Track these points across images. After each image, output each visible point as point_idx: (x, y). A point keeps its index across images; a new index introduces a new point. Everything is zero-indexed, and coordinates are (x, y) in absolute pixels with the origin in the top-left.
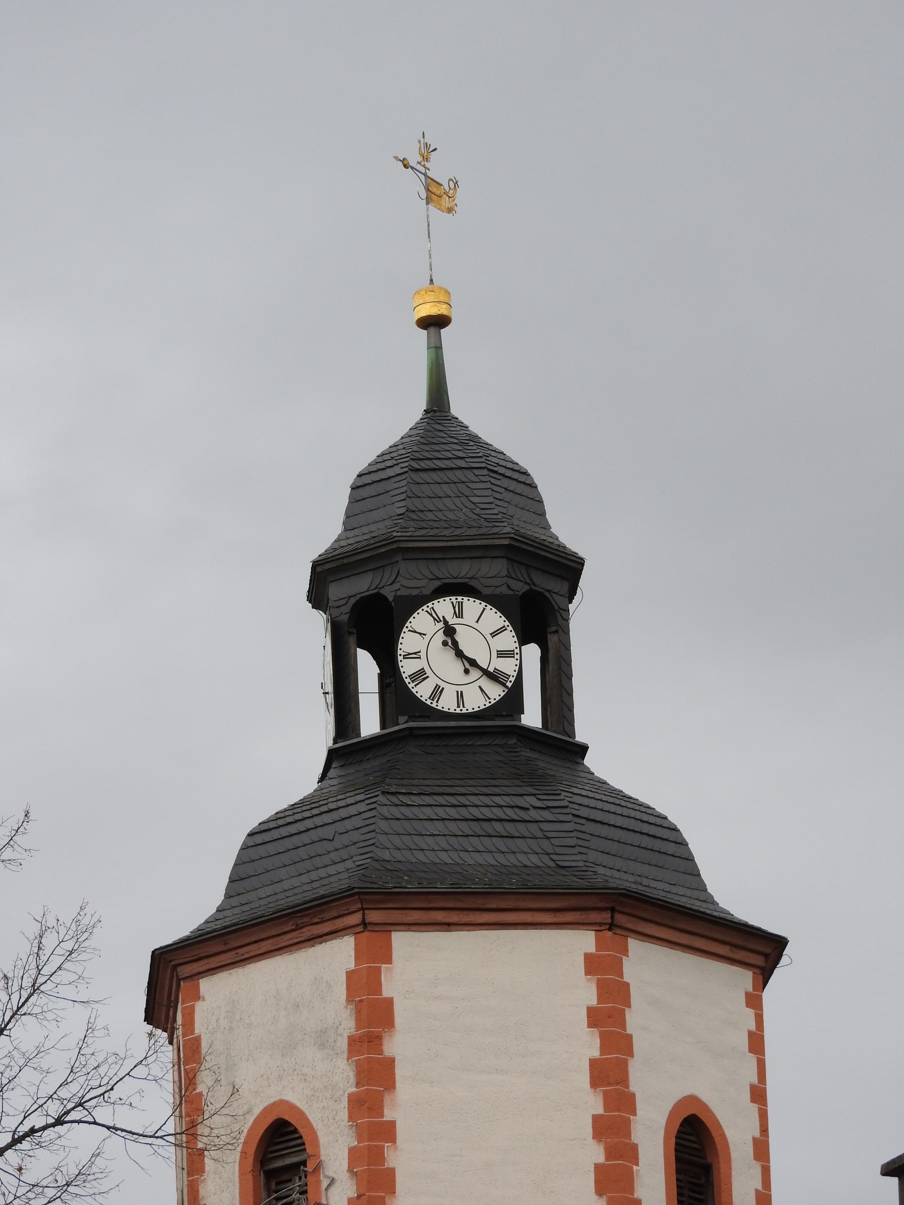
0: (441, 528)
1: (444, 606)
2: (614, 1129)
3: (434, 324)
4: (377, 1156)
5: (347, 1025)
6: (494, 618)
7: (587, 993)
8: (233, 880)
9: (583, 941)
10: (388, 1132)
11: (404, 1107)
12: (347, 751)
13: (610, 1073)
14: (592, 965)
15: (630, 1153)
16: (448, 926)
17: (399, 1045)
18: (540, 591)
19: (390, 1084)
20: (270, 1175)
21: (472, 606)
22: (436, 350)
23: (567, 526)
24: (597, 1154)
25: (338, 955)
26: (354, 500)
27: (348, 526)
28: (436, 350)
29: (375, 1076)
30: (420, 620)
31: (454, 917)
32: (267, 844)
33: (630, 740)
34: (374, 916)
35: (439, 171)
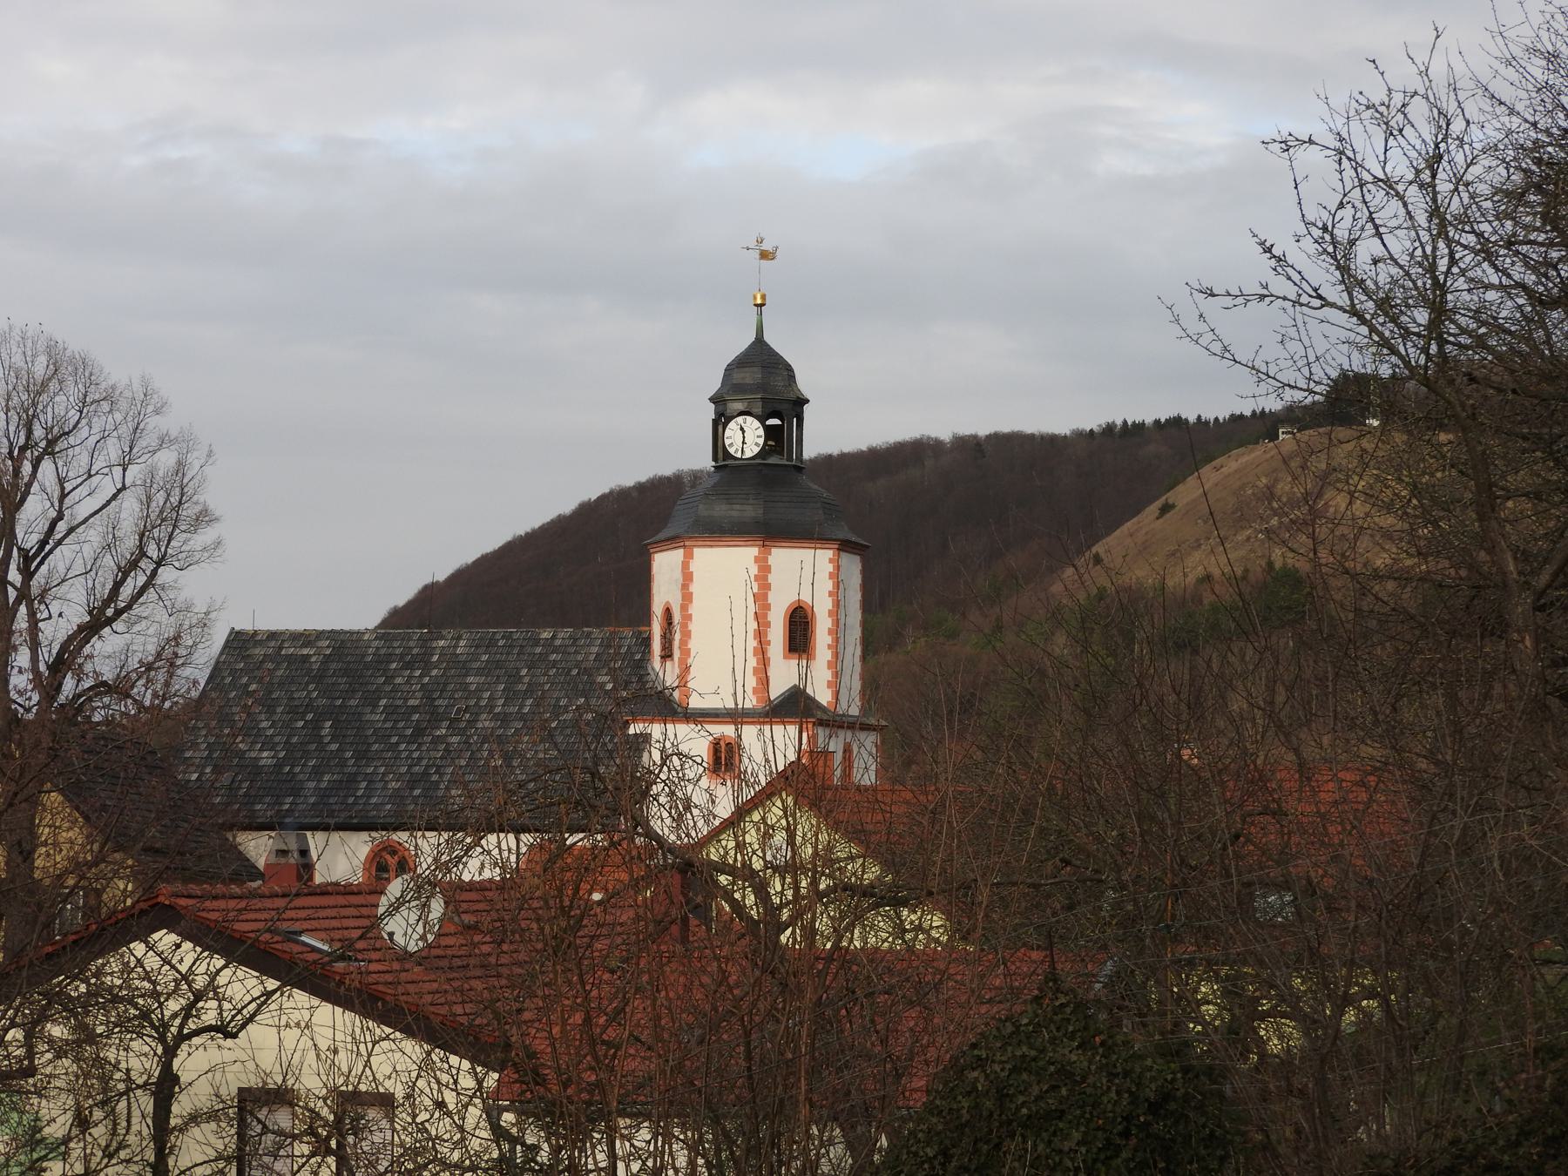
1: (740, 419)
14: (757, 560)
15: (768, 625)
17: (694, 588)
21: (750, 419)
23: (805, 383)
29: (687, 597)
30: (732, 425)
35: (766, 246)
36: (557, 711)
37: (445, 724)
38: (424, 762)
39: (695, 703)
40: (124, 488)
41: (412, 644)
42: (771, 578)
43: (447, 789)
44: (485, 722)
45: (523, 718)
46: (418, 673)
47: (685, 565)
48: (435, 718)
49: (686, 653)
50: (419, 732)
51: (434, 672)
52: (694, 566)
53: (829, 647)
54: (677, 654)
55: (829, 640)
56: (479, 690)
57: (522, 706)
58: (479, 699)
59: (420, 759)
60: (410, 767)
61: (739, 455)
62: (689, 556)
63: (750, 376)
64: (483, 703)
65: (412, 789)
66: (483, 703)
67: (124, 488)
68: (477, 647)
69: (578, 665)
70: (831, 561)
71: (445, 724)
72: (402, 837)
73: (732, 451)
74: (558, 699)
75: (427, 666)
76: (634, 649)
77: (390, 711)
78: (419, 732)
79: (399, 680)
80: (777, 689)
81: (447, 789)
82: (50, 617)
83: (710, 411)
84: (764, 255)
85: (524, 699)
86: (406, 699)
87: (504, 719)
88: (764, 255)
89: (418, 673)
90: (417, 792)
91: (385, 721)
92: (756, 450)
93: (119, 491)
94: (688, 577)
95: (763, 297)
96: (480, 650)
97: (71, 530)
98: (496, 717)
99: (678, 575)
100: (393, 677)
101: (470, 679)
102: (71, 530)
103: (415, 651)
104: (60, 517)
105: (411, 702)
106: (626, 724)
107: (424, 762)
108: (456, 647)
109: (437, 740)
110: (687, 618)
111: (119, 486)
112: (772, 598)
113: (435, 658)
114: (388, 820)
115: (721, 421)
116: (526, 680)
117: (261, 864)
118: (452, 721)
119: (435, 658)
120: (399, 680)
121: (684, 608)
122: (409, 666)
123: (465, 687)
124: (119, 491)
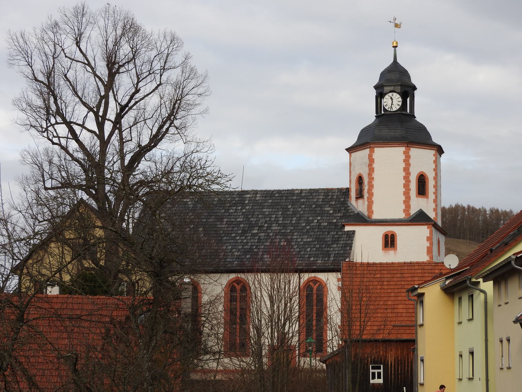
0: (396, 80)
1: (390, 94)
2: (407, 178)
3: (395, 47)
4: (371, 182)
5: (368, 162)
6: (398, 96)
7: (403, 157)
8: (358, 137)
9: (403, 149)
10: (373, 179)
11: (375, 175)
12: (379, 116)
13: (407, 170)
14: (404, 152)
15: (410, 181)
16: (383, 147)
17: (375, 166)
18: (408, 91)
19: (373, 171)
20: (359, 183)
21: (395, 94)
22: (395, 51)
23: (414, 81)
24: (404, 182)
25: (367, 151)
26: (380, 77)
27: (379, 81)
28: (395, 51)
29: (371, 170)
30: (387, 96)
31: (384, 146)
32: (364, 132)
33: (420, 116)
34: (371, 146)
35: (397, 22)
36: (308, 222)
37: (256, 228)
38: (250, 244)
39: (376, 216)
40: (161, 84)
41: (234, 196)
42: (411, 161)
43: (263, 255)
44: (275, 227)
45: (293, 225)
46: (240, 208)
47: (370, 157)
48: (252, 227)
49: (371, 194)
50: (244, 232)
51: (247, 207)
52: (375, 156)
53: (434, 193)
54: (366, 195)
55: (434, 190)
56: (270, 214)
57: (291, 220)
58: (271, 218)
59: (247, 243)
60: (243, 246)
61: (389, 110)
62: (372, 152)
63: (394, 76)
64: (273, 219)
65: (246, 255)
66: (273, 219)
67: (161, 84)
68: (266, 197)
69: (314, 203)
70: (434, 155)
71: (256, 228)
72: (242, 276)
73: (387, 108)
74: (308, 217)
75: (244, 206)
76: (340, 197)
77: (229, 223)
78: (244, 232)
79: (231, 211)
80: (413, 211)
81: (263, 255)
82: (131, 140)
83: (374, 93)
84: (397, 26)
85: (292, 217)
86: (236, 219)
87: (285, 226)
88: (397, 26)
89: (240, 208)
90: (248, 256)
91: (227, 227)
92: (398, 107)
93: (158, 85)
94: (371, 161)
95: (397, 43)
96: (267, 198)
97: (136, 103)
98: (279, 225)
99: (367, 161)
100: (229, 210)
101: (265, 210)
102: (136, 103)
103: (237, 199)
104: (137, 91)
105: (238, 220)
106: (344, 226)
107: (250, 244)
108: (256, 197)
109: (254, 235)
110: (371, 179)
111: (158, 83)
112: (411, 169)
113: (247, 202)
114: (237, 268)
115: (380, 96)
116: (292, 210)
117: (432, 218)
118: (260, 227)
119: (247, 202)
120: (231, 211)
121: (370, 175)
122: (236, 205)
123: (263, 213)
124: (158, 85)
